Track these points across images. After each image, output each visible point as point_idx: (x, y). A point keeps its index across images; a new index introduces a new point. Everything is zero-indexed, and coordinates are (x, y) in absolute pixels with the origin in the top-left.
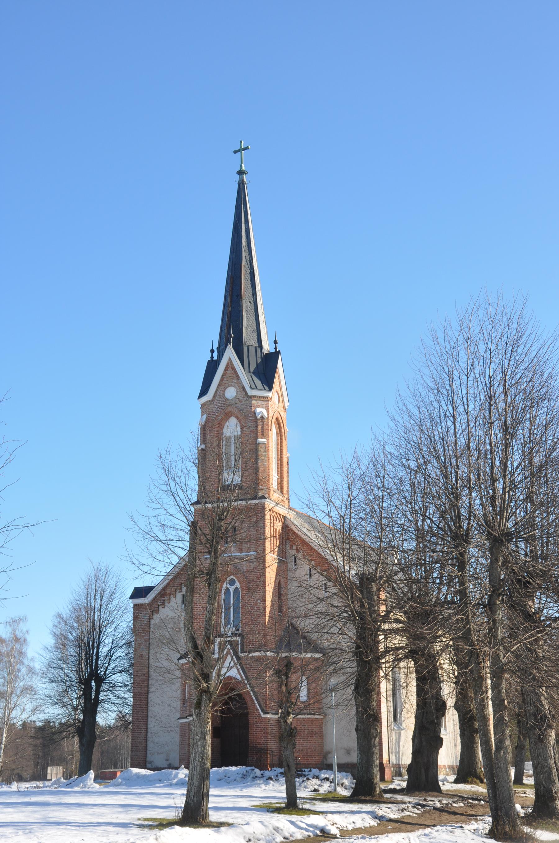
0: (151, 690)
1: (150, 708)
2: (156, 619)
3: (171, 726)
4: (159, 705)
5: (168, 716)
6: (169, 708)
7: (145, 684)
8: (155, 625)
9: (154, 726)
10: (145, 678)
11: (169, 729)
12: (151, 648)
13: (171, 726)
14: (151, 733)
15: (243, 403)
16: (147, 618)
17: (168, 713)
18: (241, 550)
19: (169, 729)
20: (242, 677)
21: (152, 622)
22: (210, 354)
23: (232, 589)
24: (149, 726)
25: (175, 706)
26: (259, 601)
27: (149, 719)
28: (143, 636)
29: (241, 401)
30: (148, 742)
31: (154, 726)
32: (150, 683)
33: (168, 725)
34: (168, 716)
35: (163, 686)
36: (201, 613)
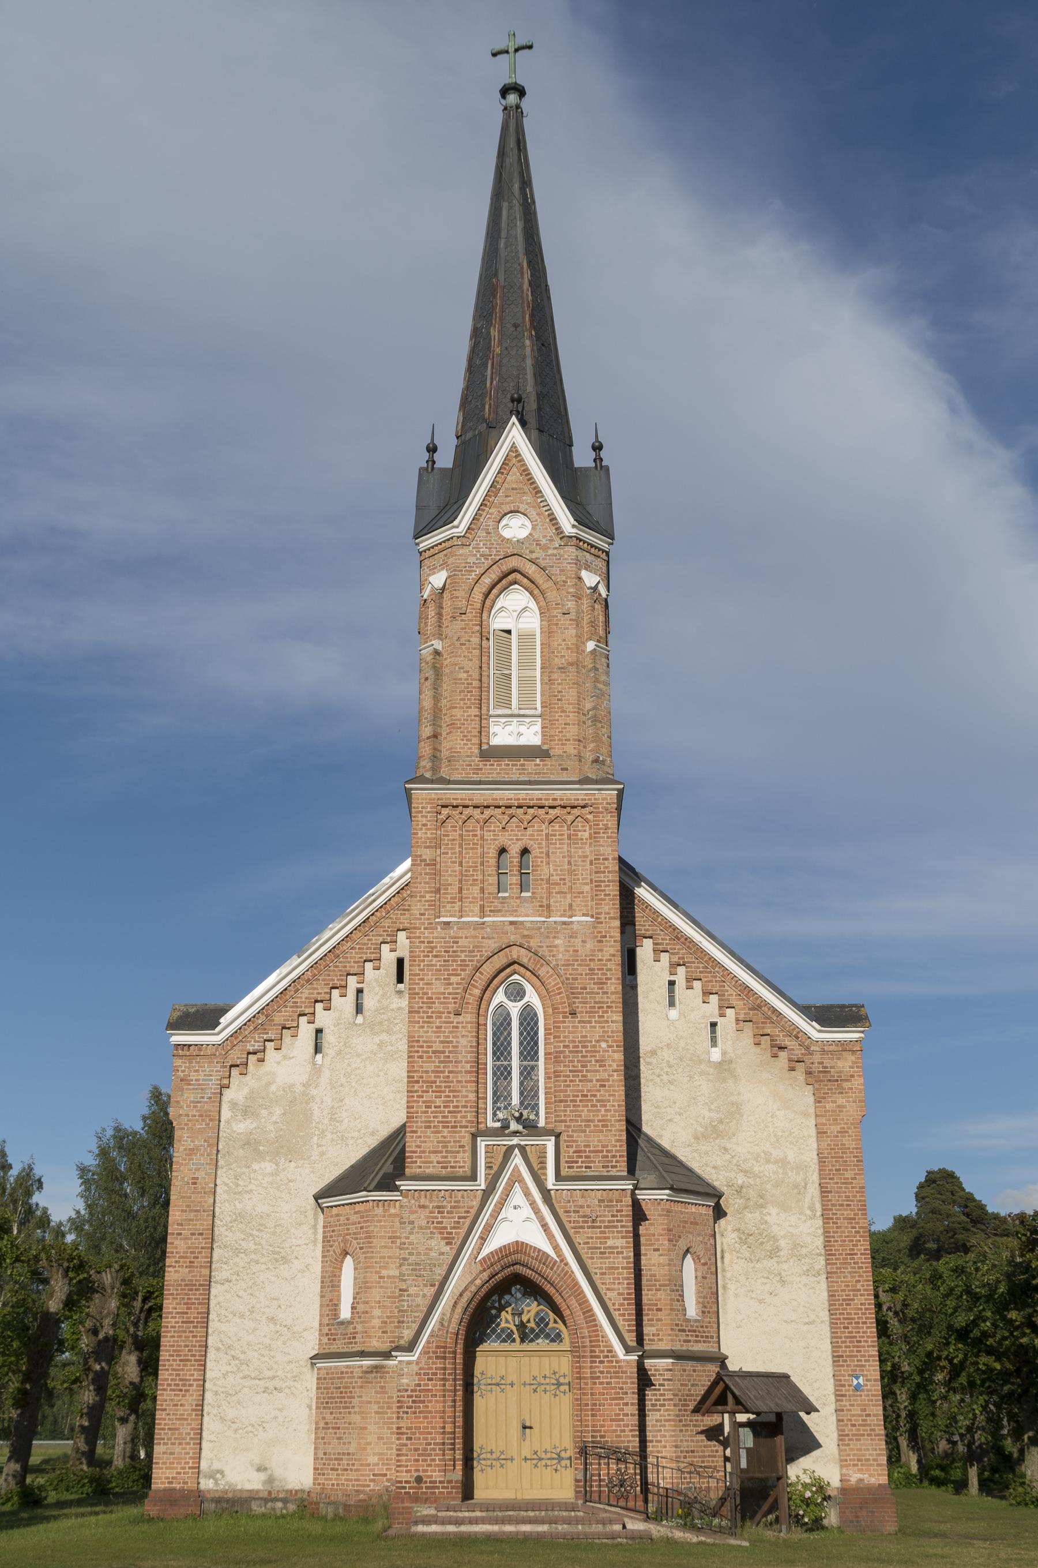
0: (220, 1274)
1: (213, 1325)
2: (237, 1092)
3: (273, 1378)
4: (242, 1316)
5: (269, 1347)
6: (272, 1327)
7: (202, 1260)
8: (234, 1105)
9: (225, 1375)
10: (202, 1242)
11: (271, 1384)
12: (221, 1162)
13: (273, 1378)
14: (216, 1393)
15: (550, 552)
16: (213, 1085)
17: (267, 1341)
18: (547, 909)
19: (271, 1384)
20: (556, 1247)
21: (228, 1095)
22: (426, 455)
23: (515, 1009)
24: (209, 1375)
25: (289, 1323)
26: (604, 1045)
27: (211, 1355)
28: (201, 1131)
29: (545, 548)
30: (206, 1419)
31: (225, 1375)
32: (215, 1257)
33: (269, 1374)
34: (269, 1347)
35: (255, 1268)
36: (431, 1067)
